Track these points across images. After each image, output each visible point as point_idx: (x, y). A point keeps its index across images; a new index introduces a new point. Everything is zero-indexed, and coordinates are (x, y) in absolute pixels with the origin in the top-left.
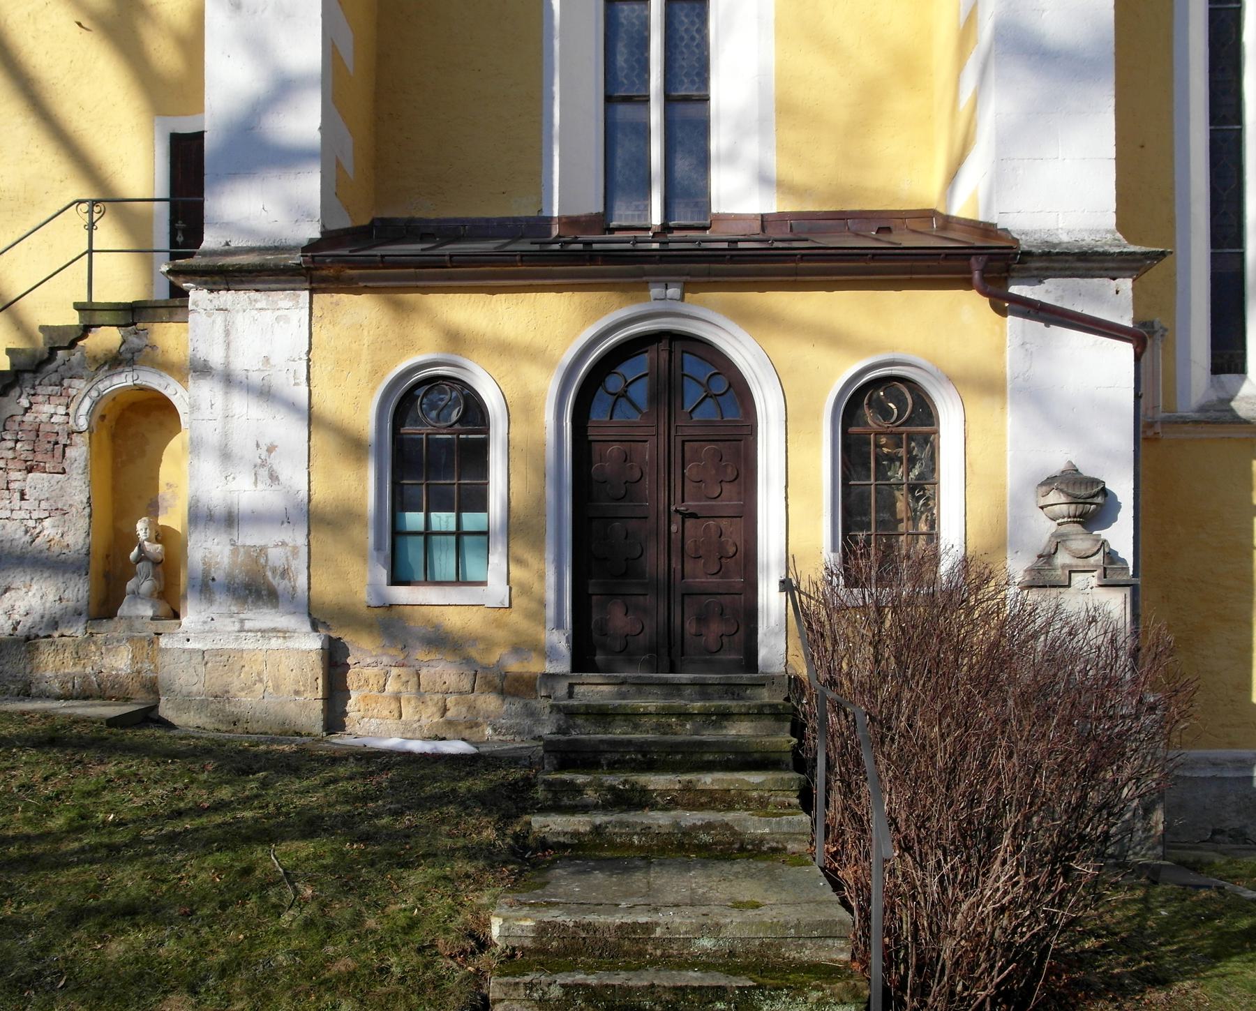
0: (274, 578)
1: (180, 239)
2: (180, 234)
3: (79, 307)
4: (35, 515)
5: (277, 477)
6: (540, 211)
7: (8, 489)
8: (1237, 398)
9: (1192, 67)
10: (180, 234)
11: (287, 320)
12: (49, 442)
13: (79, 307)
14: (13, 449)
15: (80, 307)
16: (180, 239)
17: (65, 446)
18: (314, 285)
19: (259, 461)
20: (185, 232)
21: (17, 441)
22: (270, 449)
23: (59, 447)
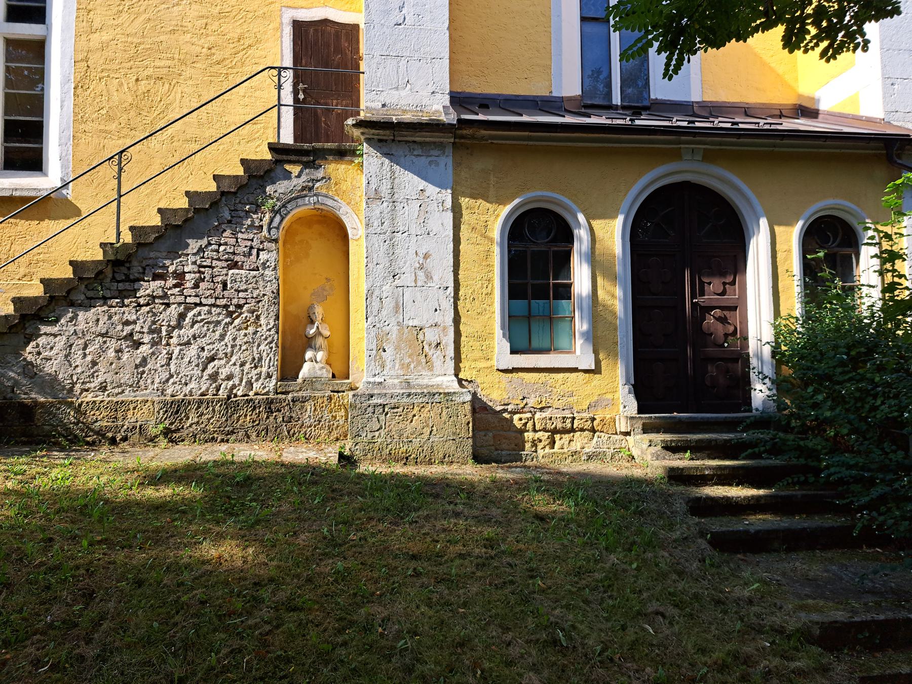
0: (430, 350)
1: (301, 96)
2: (301, 93)
3: (273, 148)
4: (235, 301)
5: (431, 278)
6: (551, 92)
7: (212, 281)
8: (396, 168)
9: (33, 26)
10: (301, 93)
11: (437, 164)
12: (246, 247)
13: (273, 148)
14: (217, 251)
15: (273, 146)
16: (301, 96)
17: (259, 250)
18: (457, 140)
19: (418, 265)
20: (304, 91)
21: (220, 245)
22: (426, 256)
23: (254, 252)
